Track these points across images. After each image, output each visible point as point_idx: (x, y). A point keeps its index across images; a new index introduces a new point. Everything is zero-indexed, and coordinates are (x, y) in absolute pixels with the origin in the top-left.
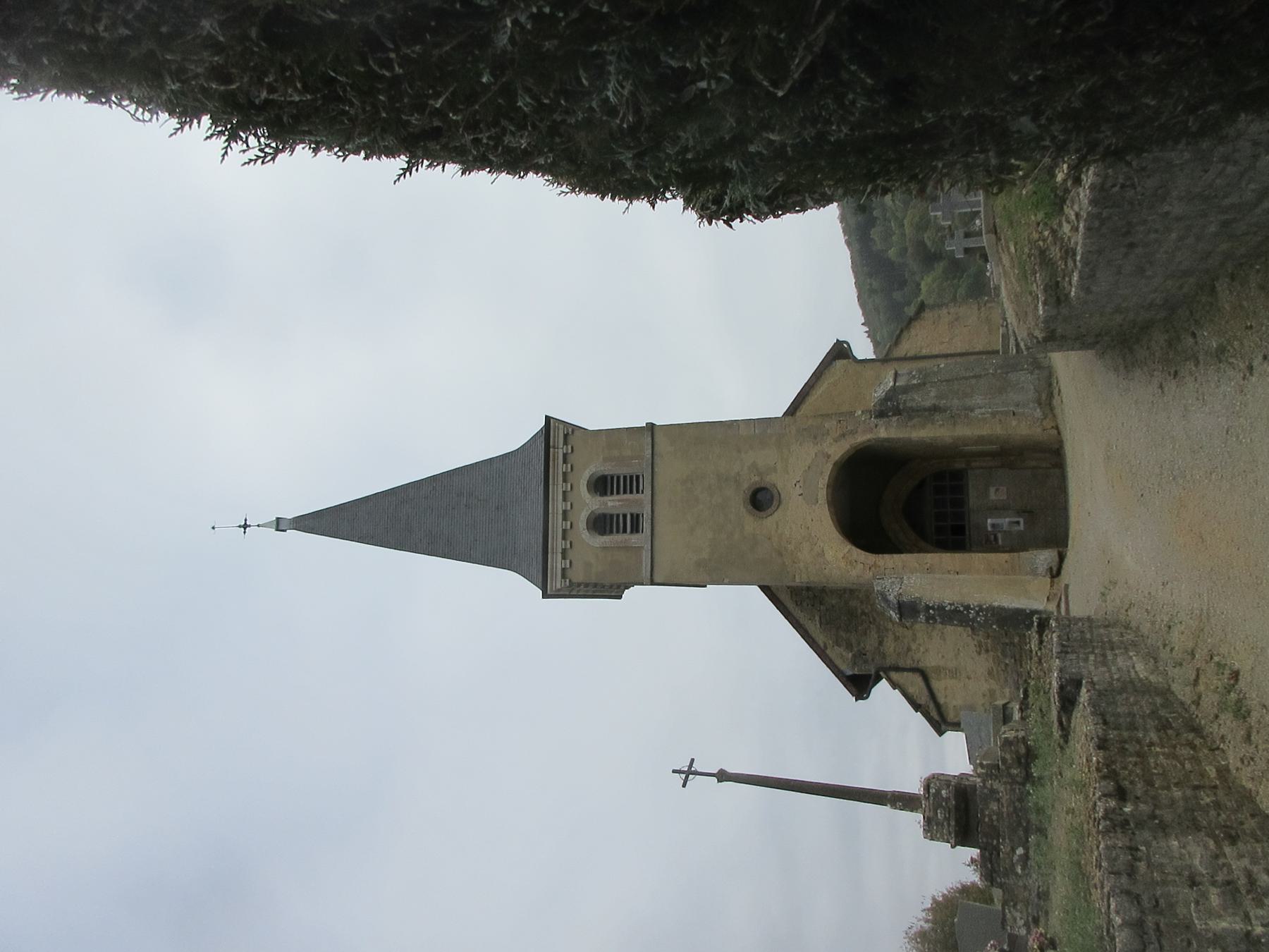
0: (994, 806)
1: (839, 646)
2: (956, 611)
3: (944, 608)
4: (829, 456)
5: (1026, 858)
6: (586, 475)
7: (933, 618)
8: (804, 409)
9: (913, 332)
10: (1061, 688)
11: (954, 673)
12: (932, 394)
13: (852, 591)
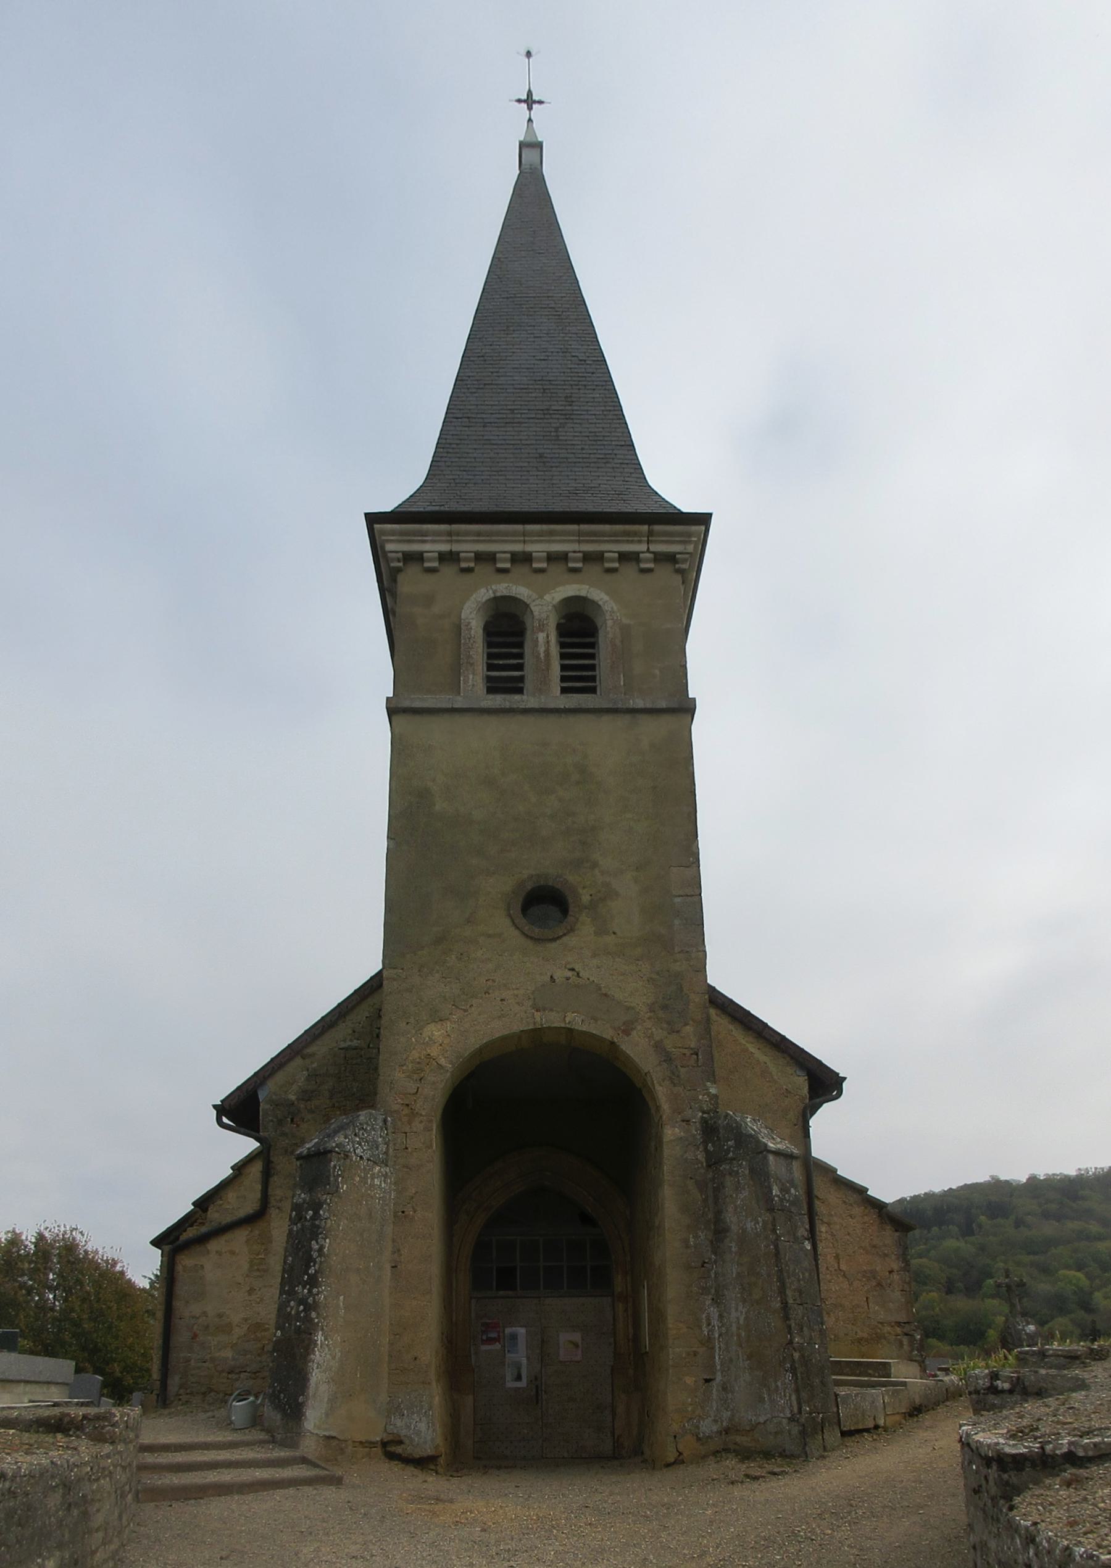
1: (309, 1078)
2: (309, 1260)
3: (315, 1235)
4: (627, 1032)
6: (598, 595)
7: (300, 1218)
8: (721, 1024)
9: (857, 1210)
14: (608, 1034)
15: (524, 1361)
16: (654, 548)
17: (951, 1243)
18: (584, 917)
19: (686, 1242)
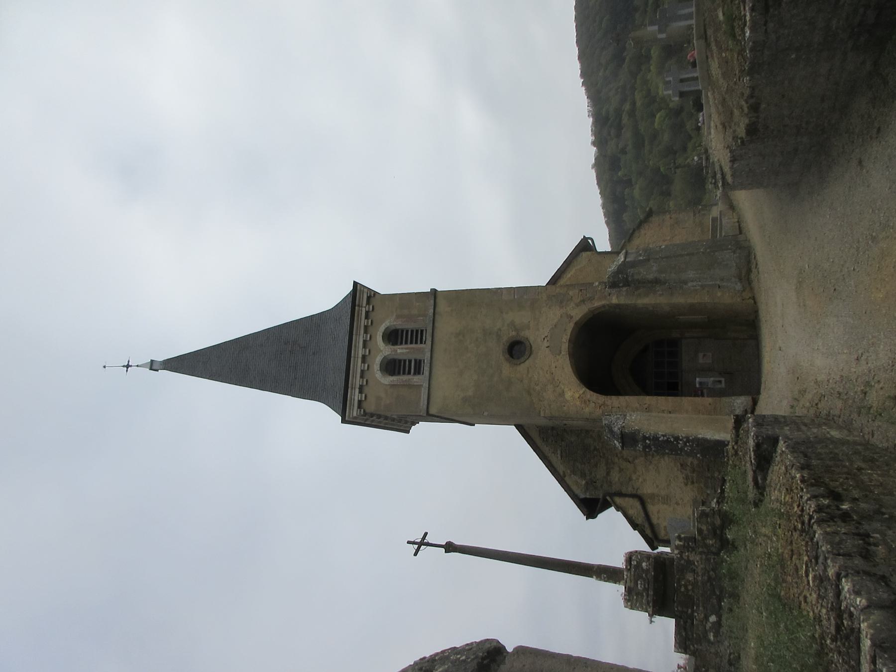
0: (690, 577)
2: (668, 441)
4: (571, 317)
5: (719, 624)
6: (382, 328)
7: (649, 446)
9: (643, 232)
10: (758, 446)
11: (666, 500)
12: (654, 268)
13: (587, 431)
14: (572, 325)
15: (712, 379)
16: (364, 305)
17: (636, 192)
18: (522, 334)
19: (660, 295)
